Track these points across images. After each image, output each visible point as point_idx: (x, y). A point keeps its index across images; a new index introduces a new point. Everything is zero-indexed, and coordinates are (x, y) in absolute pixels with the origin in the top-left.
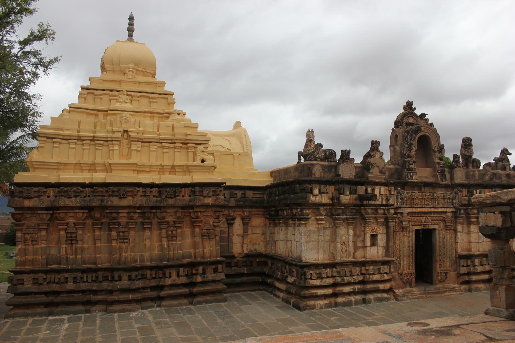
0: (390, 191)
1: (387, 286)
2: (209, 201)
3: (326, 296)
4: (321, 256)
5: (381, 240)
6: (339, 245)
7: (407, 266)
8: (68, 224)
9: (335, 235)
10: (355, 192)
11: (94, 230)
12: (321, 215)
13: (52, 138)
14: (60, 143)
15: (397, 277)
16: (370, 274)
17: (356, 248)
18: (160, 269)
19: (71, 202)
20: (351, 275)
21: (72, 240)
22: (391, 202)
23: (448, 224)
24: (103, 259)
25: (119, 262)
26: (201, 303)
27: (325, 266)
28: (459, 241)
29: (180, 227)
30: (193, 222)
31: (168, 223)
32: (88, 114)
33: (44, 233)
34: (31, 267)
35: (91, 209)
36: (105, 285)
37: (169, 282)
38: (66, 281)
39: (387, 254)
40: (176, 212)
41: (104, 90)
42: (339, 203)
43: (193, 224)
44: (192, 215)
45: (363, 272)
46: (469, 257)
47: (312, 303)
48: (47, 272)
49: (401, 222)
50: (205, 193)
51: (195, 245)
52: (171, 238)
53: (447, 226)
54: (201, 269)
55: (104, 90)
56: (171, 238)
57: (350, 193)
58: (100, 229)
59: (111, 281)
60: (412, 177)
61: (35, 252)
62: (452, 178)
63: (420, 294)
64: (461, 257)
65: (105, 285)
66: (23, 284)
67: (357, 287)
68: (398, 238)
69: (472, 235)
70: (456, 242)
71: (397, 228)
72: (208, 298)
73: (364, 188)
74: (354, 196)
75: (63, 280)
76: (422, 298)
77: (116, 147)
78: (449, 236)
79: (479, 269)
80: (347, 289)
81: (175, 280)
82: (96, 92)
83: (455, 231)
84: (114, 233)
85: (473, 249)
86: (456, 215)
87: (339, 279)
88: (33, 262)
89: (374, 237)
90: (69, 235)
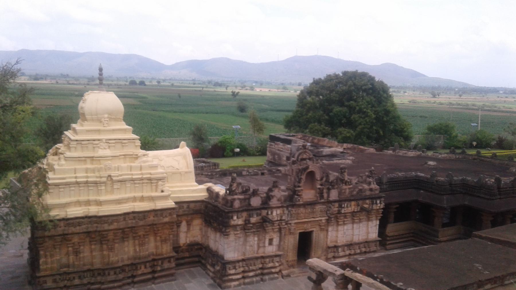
0: (283, 211)
1: (277, 270)
2: (166, 220)
3: (238, 280)
4: (236, 255)
5: (276, 241)
6: (248, 248)
7: (292, 256)
8: (73, 243)
10: (260, 214)
11: (91, 245)
12: (238, 231)
13: (59, 185)
14: (64, 188)
15: (285, 263)
16: (266, 264)
17: (259, 247)
18: (134, 266)
19: (78, 229)
20: (255, 265)
21: (77, 253)
22: (284, 218)
23: (323, 227)
24: (98, 264)
25: (108, 264)
26: (159, 283)
27: (238, 261)
28: (329, 237)
29: (147, 238)
30: (156, 234)
31: (140, 236)
32: (79, 160)
33: (58, 250)
35: (88, 233)
36: (99, 278)
37: (140, 272)
38: (74, 278)
40: (145, 229)
41: (88, 140)
42: (250, 223)
43: (155, 234)
44: (155, 229)
46: (336, 247)
47: (229, 284)
48: (60, 275)
49: (290, 229)
50: (164, 215)
51: (156, 247)
52: (142, 245)
53: (321, 229)
54: (160, 262)
55: (88, 140)
56: (142, 245)
57: (257, 216)
58: (95, 244)
59: (103, 276)
60: (299, 200)
61: (52, 262)
62: (328, 196)
63: (299, 273)
65: (99, 278)
66: (46, 283)
67: (259, 272)
68: (287, 239)
69: (339, 232)
70: (327, 238)
71: (287, 233)
72: (164, 279)
73: (266, 211)
74: (260, 217)
75: (72, 278)
76: (299, 276)
77: (103, 188)
78: (322, 235)
79: (341, 254)
80: (251, 274)
81: (143, 271)
82: (83, 142)
83: (327, 231)
84: (105, 246)
85: (338, 242)
86: (328, 221)
87: (247, 268)
88: (52, 269)
90: (75, 250)
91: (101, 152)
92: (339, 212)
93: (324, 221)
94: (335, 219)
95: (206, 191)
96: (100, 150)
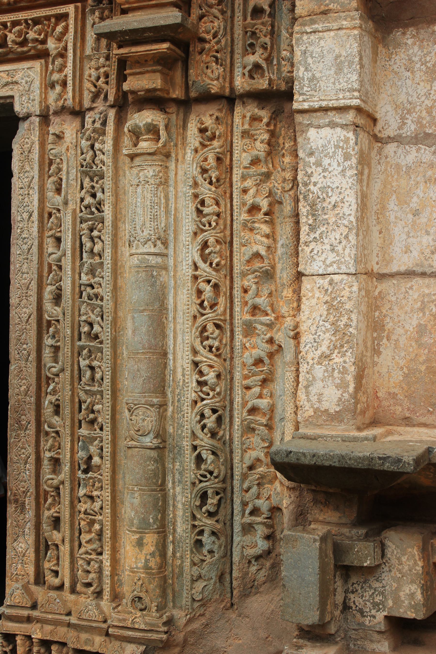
83: (278, 99)
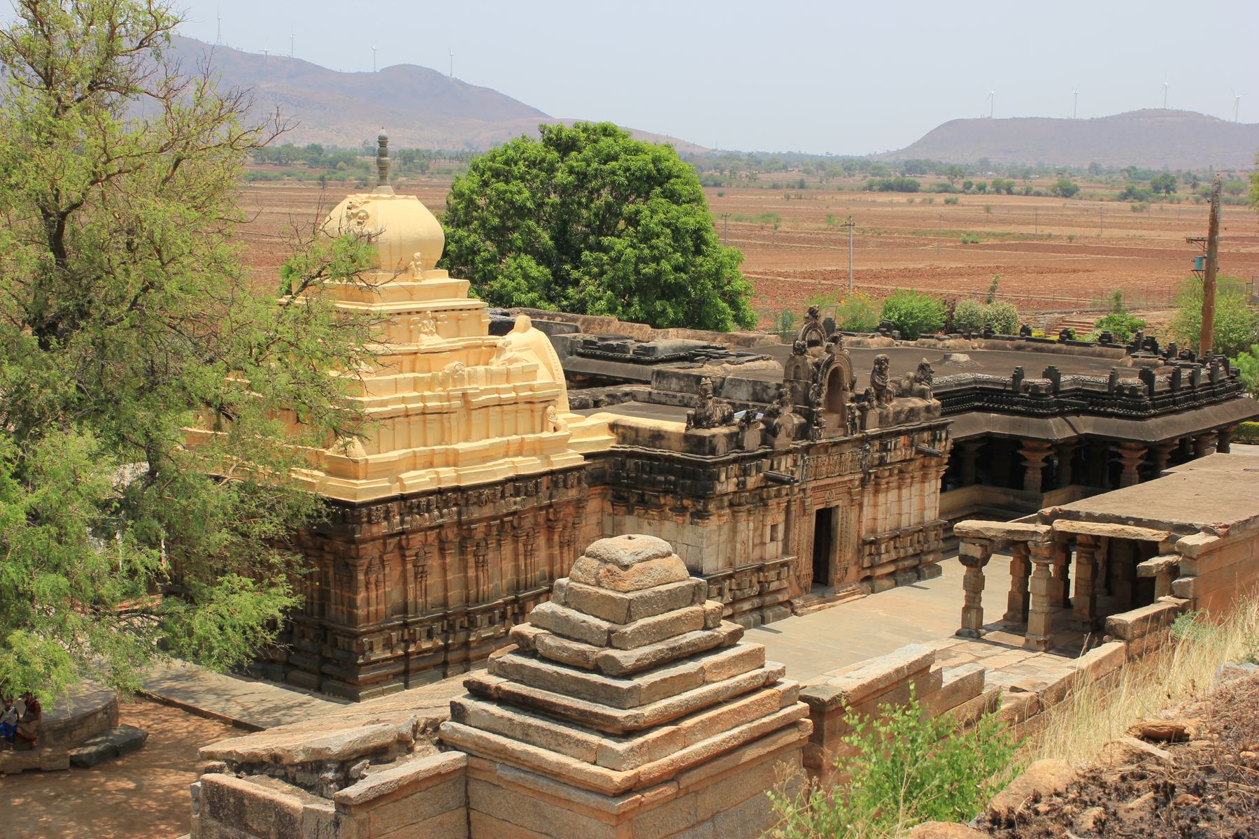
6: (738, 546)
9: (734, 531)
34: (659, 646)
39: (786, 551)
45: (406, 637)
64: (865, 543)
83: (861, 506)
86: (863, 482)
89: (774, 527)
91: (428, 341)
92: (882, 462)
93: (857, 483)
94: (871, 480)
95: (608, 430)
96: (423, 336)
